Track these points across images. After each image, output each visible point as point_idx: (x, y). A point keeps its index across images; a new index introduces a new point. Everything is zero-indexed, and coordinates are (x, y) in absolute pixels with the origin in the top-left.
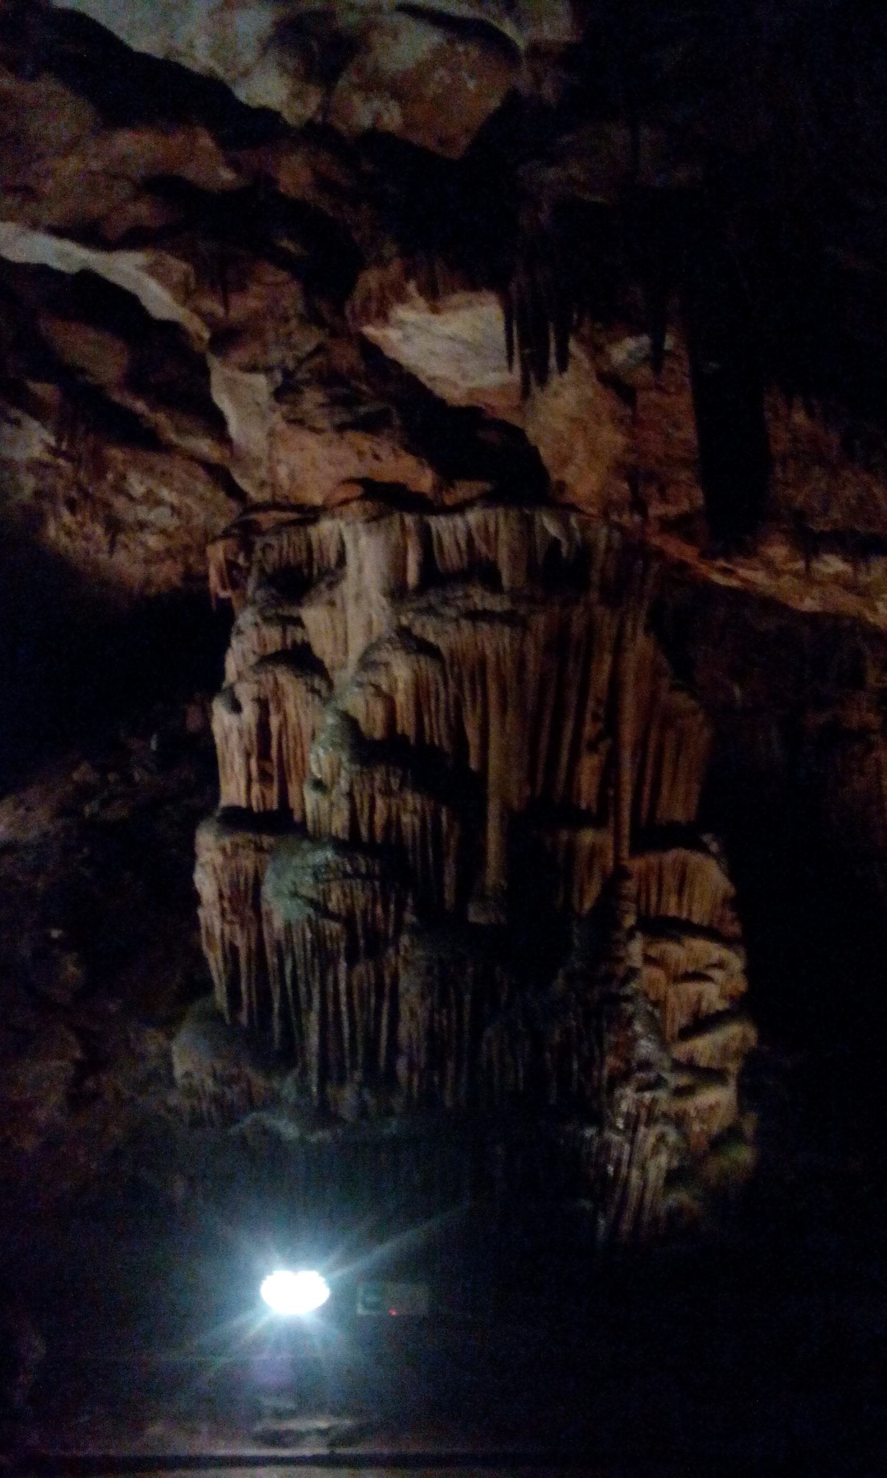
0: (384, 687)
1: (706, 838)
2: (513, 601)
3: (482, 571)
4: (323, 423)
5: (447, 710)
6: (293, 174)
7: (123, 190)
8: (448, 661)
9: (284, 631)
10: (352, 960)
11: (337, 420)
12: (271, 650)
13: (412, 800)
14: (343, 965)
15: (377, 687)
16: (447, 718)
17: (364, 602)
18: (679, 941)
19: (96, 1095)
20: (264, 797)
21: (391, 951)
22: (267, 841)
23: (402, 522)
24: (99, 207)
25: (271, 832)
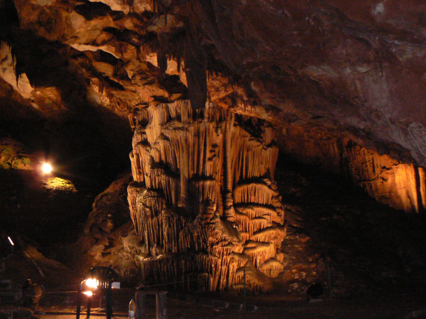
0: (158, 149)
1: (265, 180)
2: (183, 124)
3: (178, 118)
4: (140, 84)
5: (172, 152)
6: (128, 24)
7: (98, 32)
8: (171, 140)
9: (142, 135)
10: (152, 218)
11: (143, 83)
12: (139, 141)
13: (163, 177)
14: (150, 219)
15: (157, 149)
16: (172, 155)
17: (155, 127)
18: (252, 209)
19: (110, 253)
20: (140, 178)
21: (160, 215)
22: (138, 189)
23: (163, 105)
24: (94, 37)
25: (139, 187)
